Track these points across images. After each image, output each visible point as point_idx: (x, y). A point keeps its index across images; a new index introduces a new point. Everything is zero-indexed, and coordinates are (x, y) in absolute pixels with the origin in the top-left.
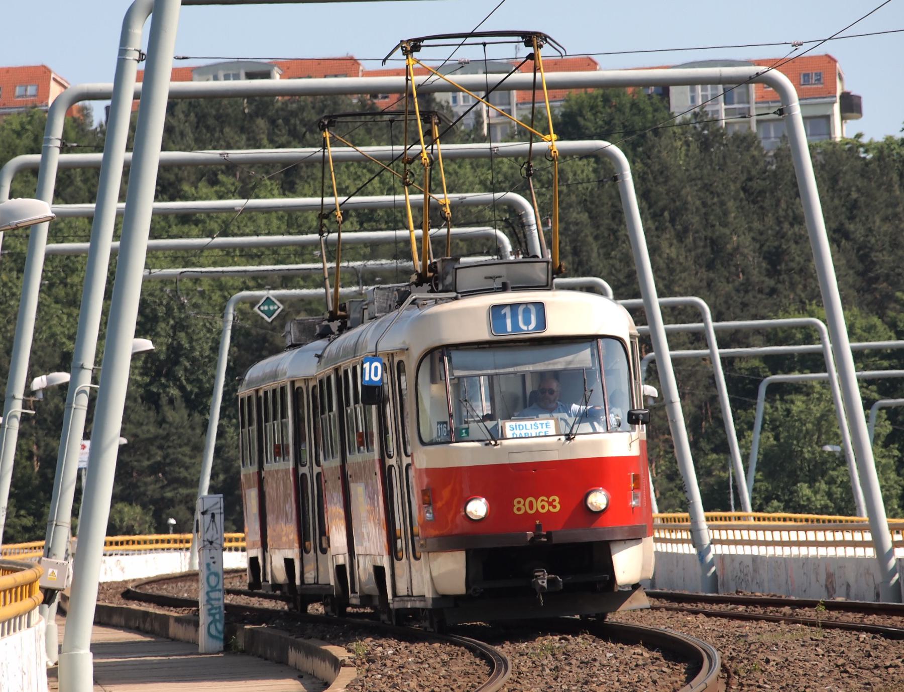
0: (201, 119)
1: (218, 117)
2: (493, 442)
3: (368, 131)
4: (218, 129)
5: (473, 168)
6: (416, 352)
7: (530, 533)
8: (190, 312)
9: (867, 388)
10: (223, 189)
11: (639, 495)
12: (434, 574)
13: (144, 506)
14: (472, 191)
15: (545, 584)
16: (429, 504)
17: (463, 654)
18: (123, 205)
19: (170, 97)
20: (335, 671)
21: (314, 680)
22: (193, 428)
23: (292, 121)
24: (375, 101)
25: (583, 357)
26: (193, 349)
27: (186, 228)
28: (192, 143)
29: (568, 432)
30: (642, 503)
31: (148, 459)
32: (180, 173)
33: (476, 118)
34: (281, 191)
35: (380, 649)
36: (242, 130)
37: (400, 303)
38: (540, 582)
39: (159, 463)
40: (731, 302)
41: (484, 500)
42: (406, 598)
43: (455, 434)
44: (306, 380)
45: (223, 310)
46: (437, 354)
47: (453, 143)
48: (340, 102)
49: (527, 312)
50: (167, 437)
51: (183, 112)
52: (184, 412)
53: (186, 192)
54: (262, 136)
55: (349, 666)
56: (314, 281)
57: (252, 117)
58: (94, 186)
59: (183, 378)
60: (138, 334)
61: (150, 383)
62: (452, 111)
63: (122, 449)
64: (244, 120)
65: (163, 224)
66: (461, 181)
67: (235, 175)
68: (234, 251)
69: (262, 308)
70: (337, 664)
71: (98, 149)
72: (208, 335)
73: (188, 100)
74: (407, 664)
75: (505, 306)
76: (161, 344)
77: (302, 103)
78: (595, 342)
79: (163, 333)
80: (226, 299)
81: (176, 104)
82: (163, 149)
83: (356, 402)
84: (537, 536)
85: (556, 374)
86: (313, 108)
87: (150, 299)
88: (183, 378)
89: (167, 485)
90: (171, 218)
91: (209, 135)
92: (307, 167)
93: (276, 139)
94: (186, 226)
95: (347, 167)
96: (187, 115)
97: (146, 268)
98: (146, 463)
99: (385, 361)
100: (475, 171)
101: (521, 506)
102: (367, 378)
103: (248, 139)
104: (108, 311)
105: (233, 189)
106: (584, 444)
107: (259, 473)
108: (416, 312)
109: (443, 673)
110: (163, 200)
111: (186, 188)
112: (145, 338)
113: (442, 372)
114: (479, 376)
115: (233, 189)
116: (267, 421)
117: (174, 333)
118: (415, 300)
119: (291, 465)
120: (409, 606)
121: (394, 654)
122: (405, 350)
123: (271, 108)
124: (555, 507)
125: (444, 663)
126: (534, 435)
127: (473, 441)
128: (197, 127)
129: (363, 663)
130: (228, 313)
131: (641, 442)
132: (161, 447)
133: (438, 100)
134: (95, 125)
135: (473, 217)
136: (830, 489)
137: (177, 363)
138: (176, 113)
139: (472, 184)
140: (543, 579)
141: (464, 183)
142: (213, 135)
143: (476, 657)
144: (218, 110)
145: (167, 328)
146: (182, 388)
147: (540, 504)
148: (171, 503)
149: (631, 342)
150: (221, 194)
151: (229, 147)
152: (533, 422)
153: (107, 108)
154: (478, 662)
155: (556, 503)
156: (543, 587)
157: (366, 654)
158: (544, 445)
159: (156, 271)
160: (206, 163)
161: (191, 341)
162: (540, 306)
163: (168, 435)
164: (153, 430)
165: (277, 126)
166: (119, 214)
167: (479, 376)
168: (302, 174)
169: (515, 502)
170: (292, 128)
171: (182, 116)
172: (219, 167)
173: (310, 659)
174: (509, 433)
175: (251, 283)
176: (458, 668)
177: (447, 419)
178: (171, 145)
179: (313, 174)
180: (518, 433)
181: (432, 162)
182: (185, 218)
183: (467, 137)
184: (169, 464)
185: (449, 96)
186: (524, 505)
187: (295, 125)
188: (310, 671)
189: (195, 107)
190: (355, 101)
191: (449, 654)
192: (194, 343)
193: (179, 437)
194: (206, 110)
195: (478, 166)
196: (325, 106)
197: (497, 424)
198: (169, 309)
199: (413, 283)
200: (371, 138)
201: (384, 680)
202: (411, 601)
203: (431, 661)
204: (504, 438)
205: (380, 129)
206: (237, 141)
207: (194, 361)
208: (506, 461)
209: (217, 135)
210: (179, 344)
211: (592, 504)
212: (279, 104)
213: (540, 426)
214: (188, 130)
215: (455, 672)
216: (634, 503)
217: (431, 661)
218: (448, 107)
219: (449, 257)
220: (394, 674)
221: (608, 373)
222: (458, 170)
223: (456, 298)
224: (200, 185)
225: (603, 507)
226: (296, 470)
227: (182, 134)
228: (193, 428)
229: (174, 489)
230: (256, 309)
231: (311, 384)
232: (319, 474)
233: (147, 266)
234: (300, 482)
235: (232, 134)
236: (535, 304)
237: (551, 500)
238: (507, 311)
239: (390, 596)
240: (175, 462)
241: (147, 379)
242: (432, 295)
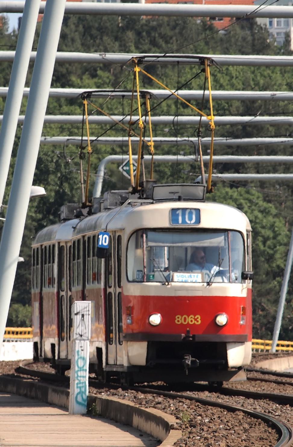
0: (87, 30)
1: (100, 29)
2: (167, 284)
3: (207, 43)
4: (99, 37)
5: (281, 73)
6: (129, 230)
7: (183, 335)
8: (73, 169)
10: (100, 81)
11: (245, 318)
12: (130, 354)
14: (280, 90)
15: (189, 363)
16: (130, 315)
17: (259, 424)
18: (28, 89)
19: (65, 13)
20: (166, 431)
21: (151, 438)
23: (153, 34)
24: (213, 22)
25: (219, 241)
27: (72, 108)
28: (79, 46)
29: (208, 281)
30: (246, 322)
32: (70, 68)
33: (285, 38)
34: (142, 84)
35: (199, 418)
36: (116, 39)
37: (122, 203)
38: (187, 361)
41: (159, 315)
42: (113, 366)
43: (143, 278)
44: (66, 243)
45: (96, 169)
46: (140, 233)
47: (268, 55)
48: (188, 22)
49: (191, 214)
51: (74, 24)
53: (73, 82)
54: (130, 44)
55: (176, 429)
56: (163, 150)
57: (124, 29)
58: (8, 75)
60: (35, 183)
61: (43, 219)
62: (268, 32)
63: (20, 265)
64: (118, 32)
65: (55, 104)
66: (273, 83)
67: (110, 71)
68: (106, 125)
69: (125, 168)
70: (168, 427)
71: (12, 47)
73: (78, 16)
74: (218, 430)
75: (178, 209)
76: (51, 190)
77: (161, 22)
78: (227, 233)
79: (52, 183)
80: (100, 160)
81: (69, 18)
82: (59, 50)
83: (93, 256)
84: (187, 337)
85: (204, 249)
86: (168, 25)
87: (44, 157)
90: (63, 100)
91: (92, 41)
92: (162, 67)
93: (140, 46)
94: (73, 106)
95: (191, 69)
96: (77, 26)
97: (42, 136)
99: (111, 234)
100: (283, 76)
101: (180, 320)
102: (100, 243)
103: (120, 46)
104: (14, 164)
105: (108, 81)
106: (216, 289)
107: (41, 293)
108: (130, 209)
109: (244, 437)
110: (57, 87)
111: (74, 78)
112: (39, 185)
113: (142, 243)
114: (164, 247)
115: (108, 81)
116: (45, 263)
117: (61, 184)
118: (130, 202)
119: (56, 290)
120: (114, 370)
121: (209, 422)
122: (123, 230)
123: (137, 23)
125: (246, 431)
127: (157, 282)
128: (84, 35)
129: (187, 427)
130: (100, 170)
131: (248, 289)
133: (259, 23)
134: (10, 30)
135: (280, 109)
138: (69, 24)
139: (280, 85)
140: (189, 360)
141: (275, 84)
142: (95, 41)
143: (269, 427)
144: (100, 24)
145: (56, 179)
147: (190, 320)
149: (247, 234)
150: (98, 84)
151: (106, 51)
152: (189, 274)
153: (20, 19)
154: (270, 430)
156: (188, 365)
157: (189, 421)
158: (194, 287)
159: (49, 139)
160: (90, 62)
161: (72, 189)
162: (198, 211)
165: (142, 37)
166: (25, 96)
167: (164, 247)
168: (158, 72)
169: (177, 317)
170: (153, 39)
171: (73, 27)
172: (98, 65)
173: (149, 423)
174: (175, 279)
175: (118, 150)
176: (255, 435)
177: (142, 269)
178: (64, 47)
179: (166, 73)
181: (145, 127)
182: (72, 101)
183: (278, 51)
185: (267, 20)
186: (181, 319)
187: (155, 38)
188: (149, 432)
189: (83, 21)
190: (199, 22)
191: (249, 424)
192: (74, 192)
194: (91, 24)
195: (285, 72)
196: (177, 25)
197: (170, 274)
198: (58, 164)
199: (130, 192)
200: (209, 49)
201: (202, 441)
202: (116, 367)
203: (236, 428)
204: (172, 281)
205: (216, 42)
206: (113, 47)
208: (172, 294)
209: (98, 41)
211: (218, 321)
212: (144, 22)
214: (77, 36)
215: (253, 437)
216: (241, 322)
217: (236, 428)
218: (265, 29)
219: (152, 180)
220: (209, 436)
221: (233, 250)
222: (271, 75)
223: (152, 203)
224: (84, 77)
225: (224, 323)
226: (58, 293)
227: (73, 40)
230: (120, 168)
231: (69, 245)
232: (119, 293)
233: (43, 134)
234: (60, 300)
235: (109, 40)
236: (195, 209)
237: (196, 317)
238: (180, 212)
239: (104, 364)
241: (40, 216)
242: (140, 201)
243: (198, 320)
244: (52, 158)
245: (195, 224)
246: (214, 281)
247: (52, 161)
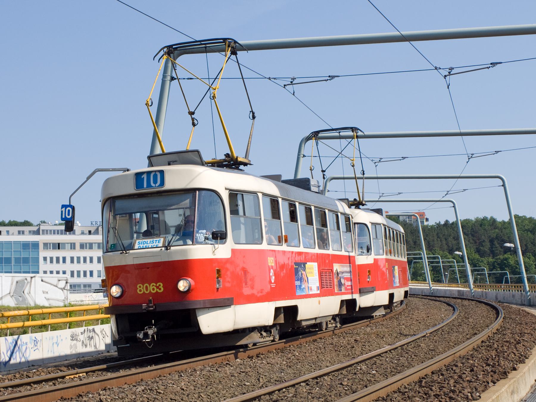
106: (176, 252)
124: (160, 289)
147: (151, 288)
152: (151, 240)
155: (161, 287)
156: (139, 338)
162: (162, 172)
169: (138, 287)
186: (143, 288)
213: (155, 242)
216: (368, 280)
237: (158, 285)
243: (160, 287)
245: (160, 186)
246: (172, 245)
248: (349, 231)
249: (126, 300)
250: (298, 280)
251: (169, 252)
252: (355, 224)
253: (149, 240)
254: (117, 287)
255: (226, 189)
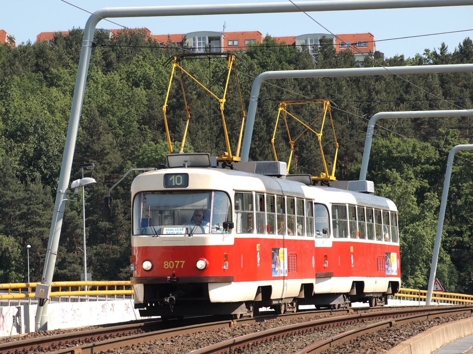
9: (422, 181)
13: (15, 237)
22: (45, 194)
26: (48, 151)
31: (19, 211)
39: (25, 213)
40: (345, 133)
50: (29, 199)
52: (41, 185)
59: (42, 167)
61: (24, 169)
72: (57, 143)
88: (42, 167)
89: (29, 226)
98: (18, 213)
126: (175, 233)
132: (26, 204)
136: (405, 236)
137: (40, 158)
146: (42, 172)
148: (31, 235)
152: (177, 228)
156: (167, 302)
163: (30, 198)
164: (22, 194)
174: (165, 232)
180: (169, 232)
184: (31, 214)
186: (169, 264)
192: (49, 148)
193: (36, 199)
207: (49, 158)
210: (41, 148)
213: (179, 230)
228: (45, 194)
229: (32, 228)
240: (34, 213)
241: (22, 167)
244: (31, 123)
247: (32, 126)
248: (311, 215)
249: (156, 274)
250: (273, 264)
251: (192, 238)
252: (315, 203)
253: (174, 229)
254: (150, 268)
255: (234, 190)
